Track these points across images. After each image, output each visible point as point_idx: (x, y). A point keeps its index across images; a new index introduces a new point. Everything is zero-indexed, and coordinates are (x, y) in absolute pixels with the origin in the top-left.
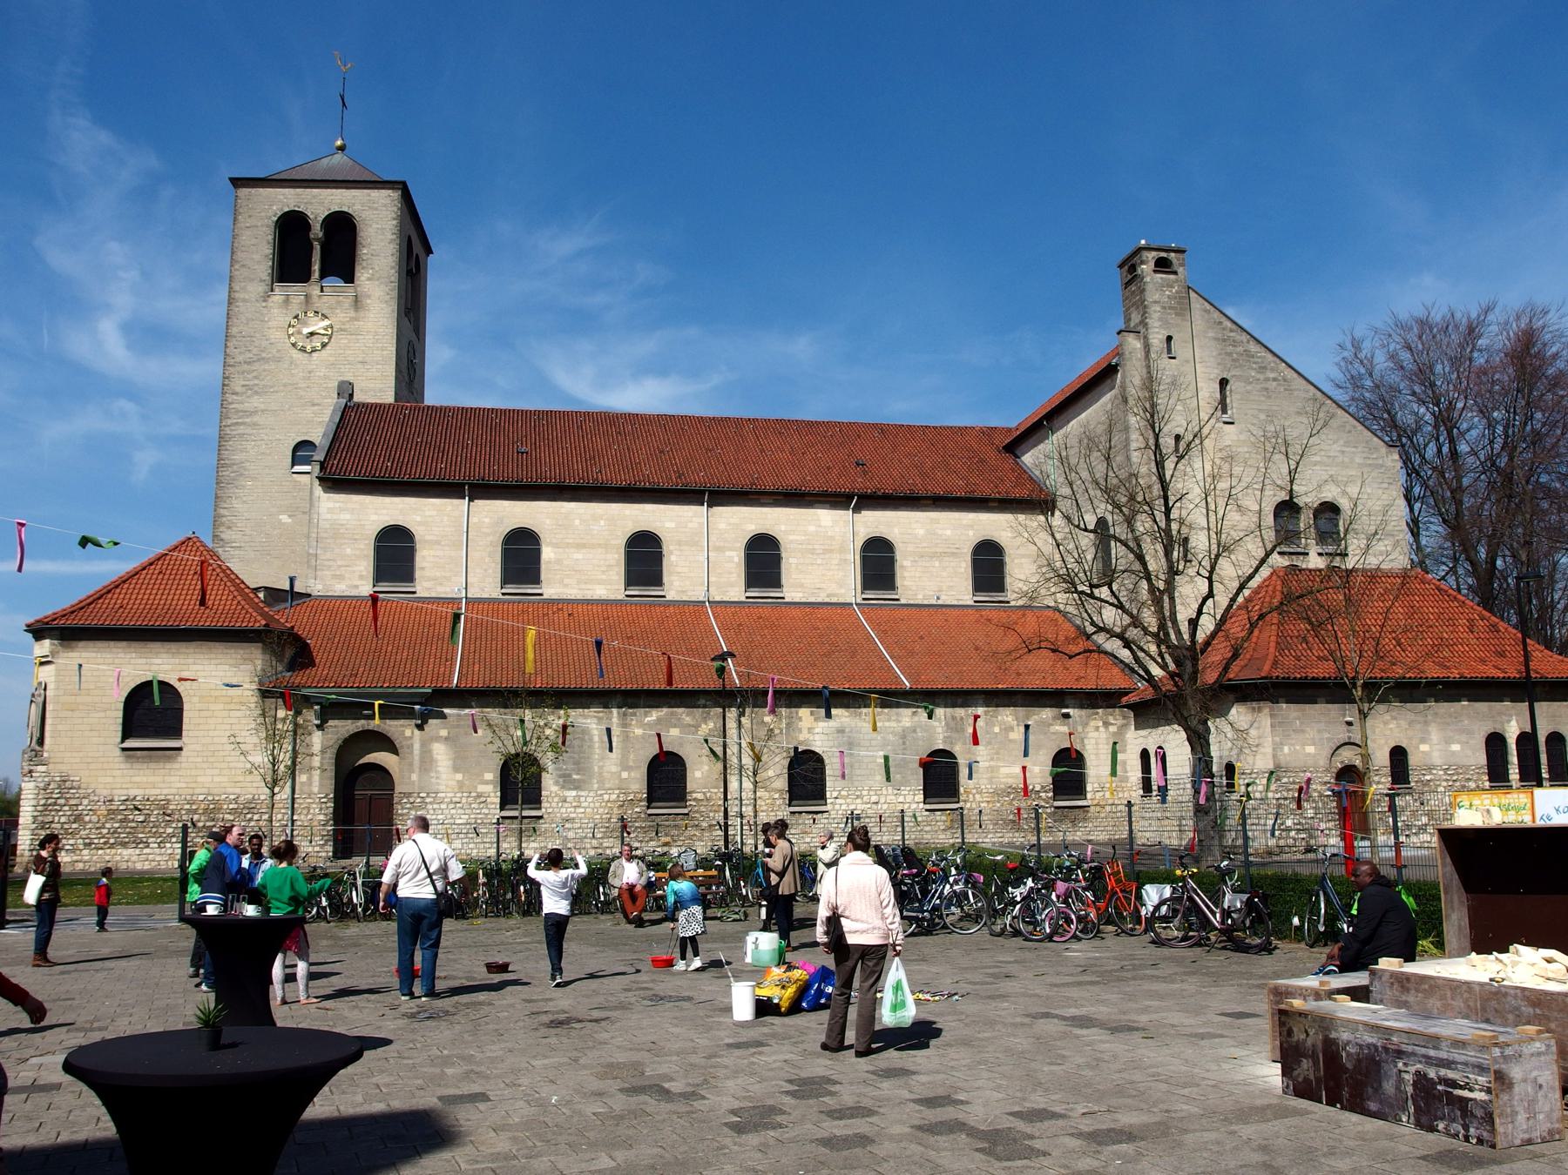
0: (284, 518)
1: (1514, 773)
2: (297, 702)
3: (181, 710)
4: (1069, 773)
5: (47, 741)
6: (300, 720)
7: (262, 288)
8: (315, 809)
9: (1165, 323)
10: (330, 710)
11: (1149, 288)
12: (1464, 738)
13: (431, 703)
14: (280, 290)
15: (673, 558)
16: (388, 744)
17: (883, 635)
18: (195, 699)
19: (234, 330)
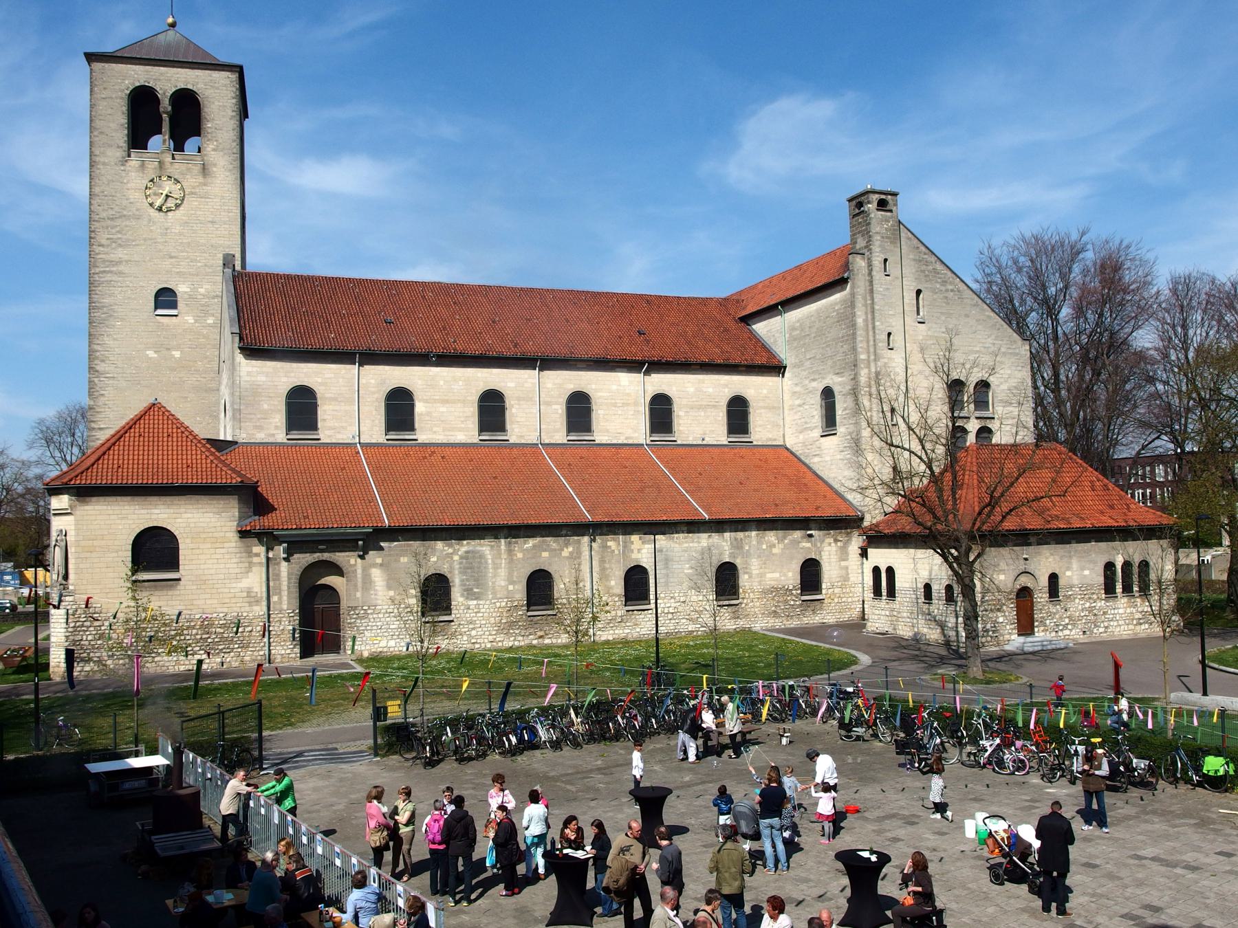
0: (151, 354)
1: (1119, 588)
2: (268, 538)
3: (178, 548)
4: (811, 575)
5: (72, 576)
6: (271, 555)
7: (120, 153)
8: (285, 622)
9: (883, 249)
10: (296, 545)
11: (873, 222)
12: (1091, 566)
13: (370, 540)
15: (514, 410)
16: (337, 570)
17: (672, 470)
18: (188, 541)
19: (97, 190)
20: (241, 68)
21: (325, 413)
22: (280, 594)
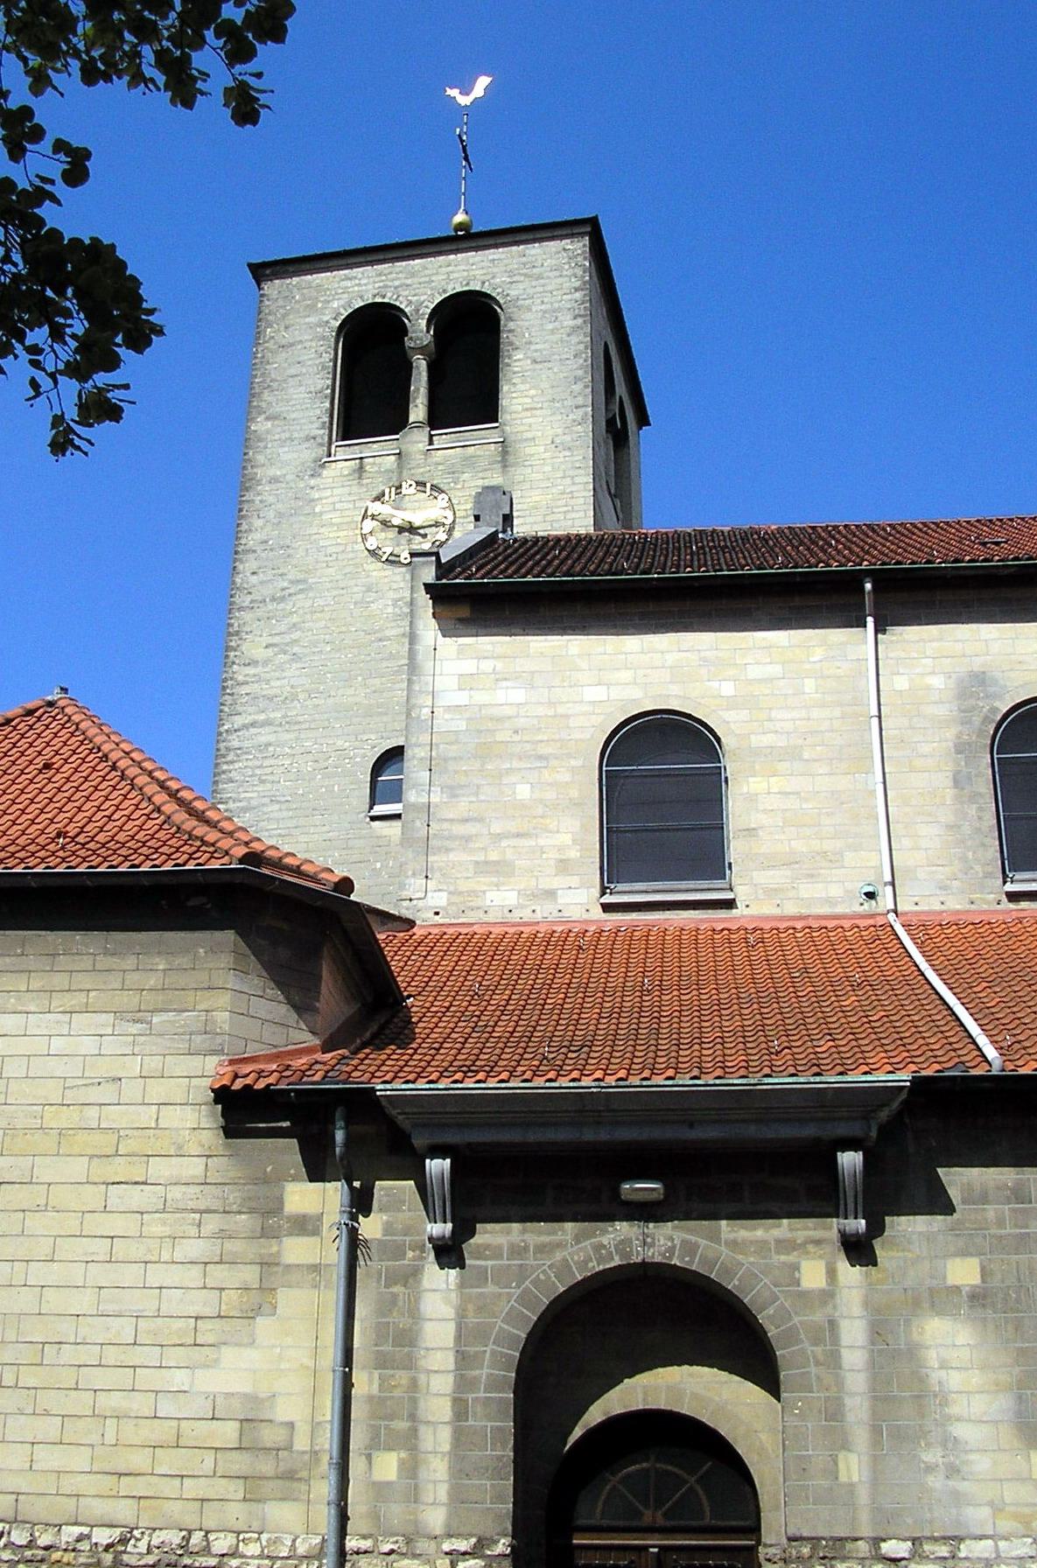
7: (310, 453)
10: (509, 1167)
14: (346, 452)
16: (729, 1332)
20: (593, 223)
21: (756, 804)
22: (409, 1441)
